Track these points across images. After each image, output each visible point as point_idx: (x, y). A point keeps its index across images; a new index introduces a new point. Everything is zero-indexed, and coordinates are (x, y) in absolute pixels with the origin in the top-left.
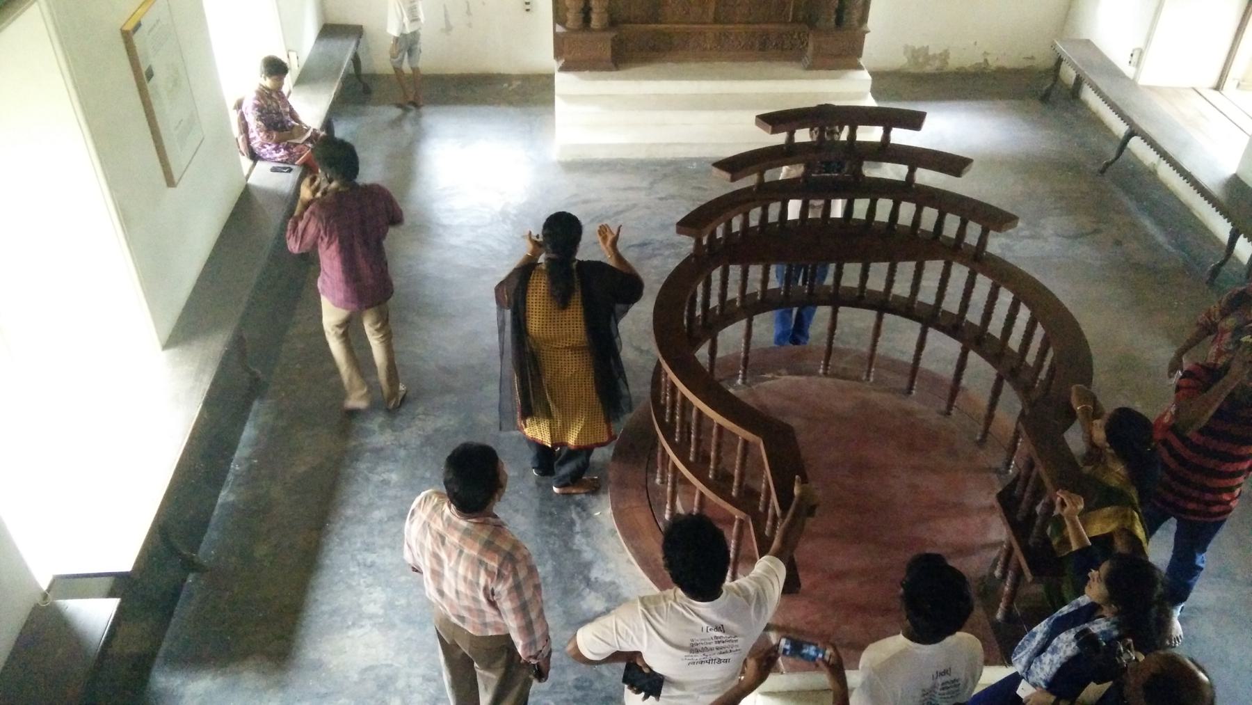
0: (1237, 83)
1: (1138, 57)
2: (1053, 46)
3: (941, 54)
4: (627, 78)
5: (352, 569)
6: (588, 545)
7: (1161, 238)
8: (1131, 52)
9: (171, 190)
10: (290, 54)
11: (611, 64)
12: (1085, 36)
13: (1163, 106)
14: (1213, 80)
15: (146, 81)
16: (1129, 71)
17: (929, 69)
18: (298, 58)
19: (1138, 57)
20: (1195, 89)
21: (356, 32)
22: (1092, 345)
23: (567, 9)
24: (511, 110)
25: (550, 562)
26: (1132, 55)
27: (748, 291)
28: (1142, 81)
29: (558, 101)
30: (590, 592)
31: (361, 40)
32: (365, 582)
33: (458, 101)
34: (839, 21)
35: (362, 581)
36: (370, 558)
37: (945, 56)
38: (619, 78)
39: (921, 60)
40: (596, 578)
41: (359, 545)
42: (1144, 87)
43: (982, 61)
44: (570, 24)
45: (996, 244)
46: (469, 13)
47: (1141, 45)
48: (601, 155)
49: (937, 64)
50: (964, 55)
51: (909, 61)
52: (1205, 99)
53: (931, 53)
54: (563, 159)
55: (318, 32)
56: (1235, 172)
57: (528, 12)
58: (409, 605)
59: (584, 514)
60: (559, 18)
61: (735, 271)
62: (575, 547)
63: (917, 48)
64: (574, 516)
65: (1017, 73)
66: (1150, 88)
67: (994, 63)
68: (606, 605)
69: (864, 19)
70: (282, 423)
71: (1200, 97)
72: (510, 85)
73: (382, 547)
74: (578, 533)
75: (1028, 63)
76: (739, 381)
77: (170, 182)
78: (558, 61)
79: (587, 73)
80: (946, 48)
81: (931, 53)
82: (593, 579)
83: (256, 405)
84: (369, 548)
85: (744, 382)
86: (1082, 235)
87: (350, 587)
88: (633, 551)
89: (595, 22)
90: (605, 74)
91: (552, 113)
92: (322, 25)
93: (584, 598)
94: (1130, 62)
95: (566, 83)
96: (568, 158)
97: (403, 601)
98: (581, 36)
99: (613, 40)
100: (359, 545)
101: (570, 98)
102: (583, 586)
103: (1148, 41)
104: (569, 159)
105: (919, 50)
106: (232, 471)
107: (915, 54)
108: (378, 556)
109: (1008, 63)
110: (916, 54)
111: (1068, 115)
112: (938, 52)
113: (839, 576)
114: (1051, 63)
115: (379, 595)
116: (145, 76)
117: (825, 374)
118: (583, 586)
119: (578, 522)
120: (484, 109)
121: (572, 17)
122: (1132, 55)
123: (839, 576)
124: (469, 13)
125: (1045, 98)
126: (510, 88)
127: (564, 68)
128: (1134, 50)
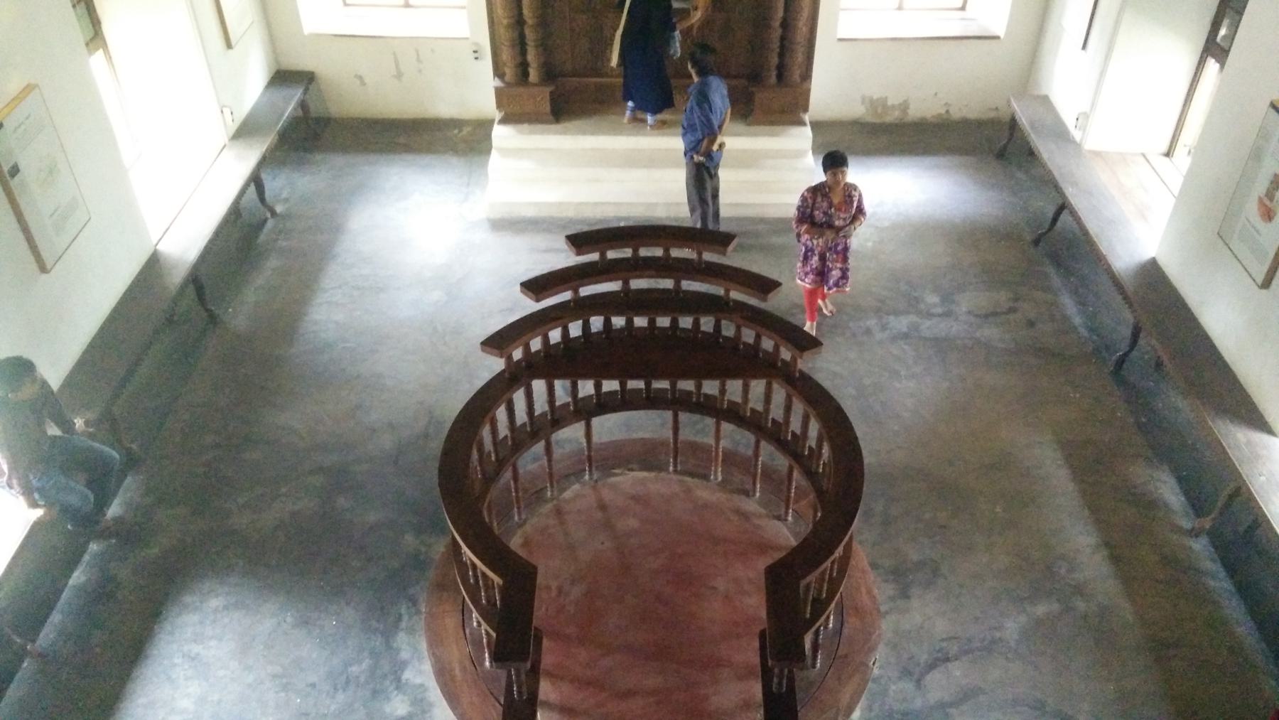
0: (1187, 151)
1: (1083, 118)
2: (1009, 102)
3: (900, 104)
4: (564, 133)
5: (176, 661)
6: (409, 644)
7: (1077, 320)
8: (1077, 117)
9: (44, 276)
10: (224, 110)
11: (551, 117)
12: (1044, 92)
13: (1102, 176)
14: (1165, 148)
15: (9, 178)
16: (1076, 135)
17: (889, 119)
18: (232, 113)
19: (1083, 118)
20: (1144, 155)
21: (306, 79)
22: (461, 638)
23: (505, 64)
24: (454, 160)
25: (367, 660)
26: (1077, 119)
27: (581, 395)
28: (1089, 145)
29: (494, 152)
30: (397, 695)
31: (311, 87)
32: (184, 675)
33: (408, 149)
34: (780, 76)
35: (182, 673)
36: (196, 649)
37: (904, 107)
38: (557, 133)
39: (879, 111)
40: (407, 680)
41: (189, 635)
42: (1090, 152)
43: (943, 111)
44: (508, 78)
45: (806, 364)
46: (419, 60)
47: (1086, 108)
48: (530, 213)
49: (897, 113)
50: (924, 106)
51: (867, 110)
52: (1153, 168)
53: (889, 103)
54: (492, 216)
55: (270, 78)
56: (1153, 256)
57: (475, 60)
58: (219, 702)
59: (413, 610)
60: (498, 72)
61: (539, 386)
62: (395, 645)
63: (875, 97)
64: (403, 611)
65: (980, 124)
66: (1097, 154)
67: (956, 114)
68: (410, 709)
69: (807, 75)
70: (149, 500)
71: (1147, 164)
72: (460, 131)
73: (211, 638)
74: (402, 630)
75: (992, 115)
76: (587, 477)
77: (43, 269)
78: (500, 111)
79: (526, 126)
80: (905, 98)
81: (889, 103)
82: (404, 681)
83: (129, 480)
84: (197, 639)
85: (591, 479)
86: (995, 314)
87: (169, 678)
88: (433, 660)
89: (533, 75)
90: (540, 127)
91: (485, 165)
92: (273, 71)
93: (388, 699)
94: (1076, 127)
95: (502, 134)
96: (496, 215)
97: (216, 697)
98: (521, 90)
99: (551, 93)
100: (189, 635)
101: (506, 152)
102: (391, 688)
103: (1093, 105)
104: (498, 216)
105: (878, 100)
106: (90, 550)
107: (873, 104)
108: (204, 648)
109: (972, 115)
110: (876, 105)
111: (1020, 175)
112: (896, 103)
113: (628, 694)
114: (1008, 119)
115: (195, 688)
116: (7, 176)
117: (675, 471)
118: (391, 688)
119: (405, 618)
120: (427, 159)
121: (509, 72)
122: (1077, 119)
123: (628, 694)
124: (419, 60)
125: (1001, 155)
126: (461, 134)
127: (504, 121)
128: (1079, 114)
